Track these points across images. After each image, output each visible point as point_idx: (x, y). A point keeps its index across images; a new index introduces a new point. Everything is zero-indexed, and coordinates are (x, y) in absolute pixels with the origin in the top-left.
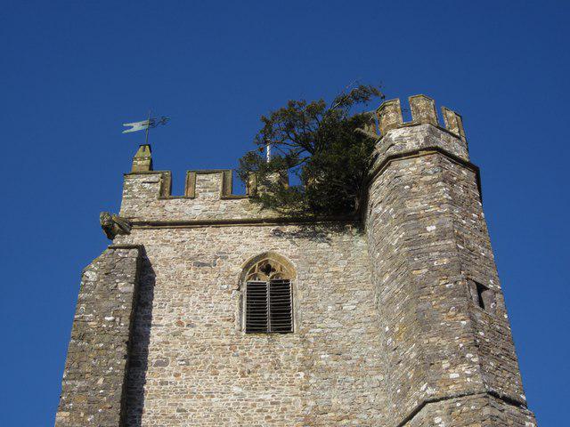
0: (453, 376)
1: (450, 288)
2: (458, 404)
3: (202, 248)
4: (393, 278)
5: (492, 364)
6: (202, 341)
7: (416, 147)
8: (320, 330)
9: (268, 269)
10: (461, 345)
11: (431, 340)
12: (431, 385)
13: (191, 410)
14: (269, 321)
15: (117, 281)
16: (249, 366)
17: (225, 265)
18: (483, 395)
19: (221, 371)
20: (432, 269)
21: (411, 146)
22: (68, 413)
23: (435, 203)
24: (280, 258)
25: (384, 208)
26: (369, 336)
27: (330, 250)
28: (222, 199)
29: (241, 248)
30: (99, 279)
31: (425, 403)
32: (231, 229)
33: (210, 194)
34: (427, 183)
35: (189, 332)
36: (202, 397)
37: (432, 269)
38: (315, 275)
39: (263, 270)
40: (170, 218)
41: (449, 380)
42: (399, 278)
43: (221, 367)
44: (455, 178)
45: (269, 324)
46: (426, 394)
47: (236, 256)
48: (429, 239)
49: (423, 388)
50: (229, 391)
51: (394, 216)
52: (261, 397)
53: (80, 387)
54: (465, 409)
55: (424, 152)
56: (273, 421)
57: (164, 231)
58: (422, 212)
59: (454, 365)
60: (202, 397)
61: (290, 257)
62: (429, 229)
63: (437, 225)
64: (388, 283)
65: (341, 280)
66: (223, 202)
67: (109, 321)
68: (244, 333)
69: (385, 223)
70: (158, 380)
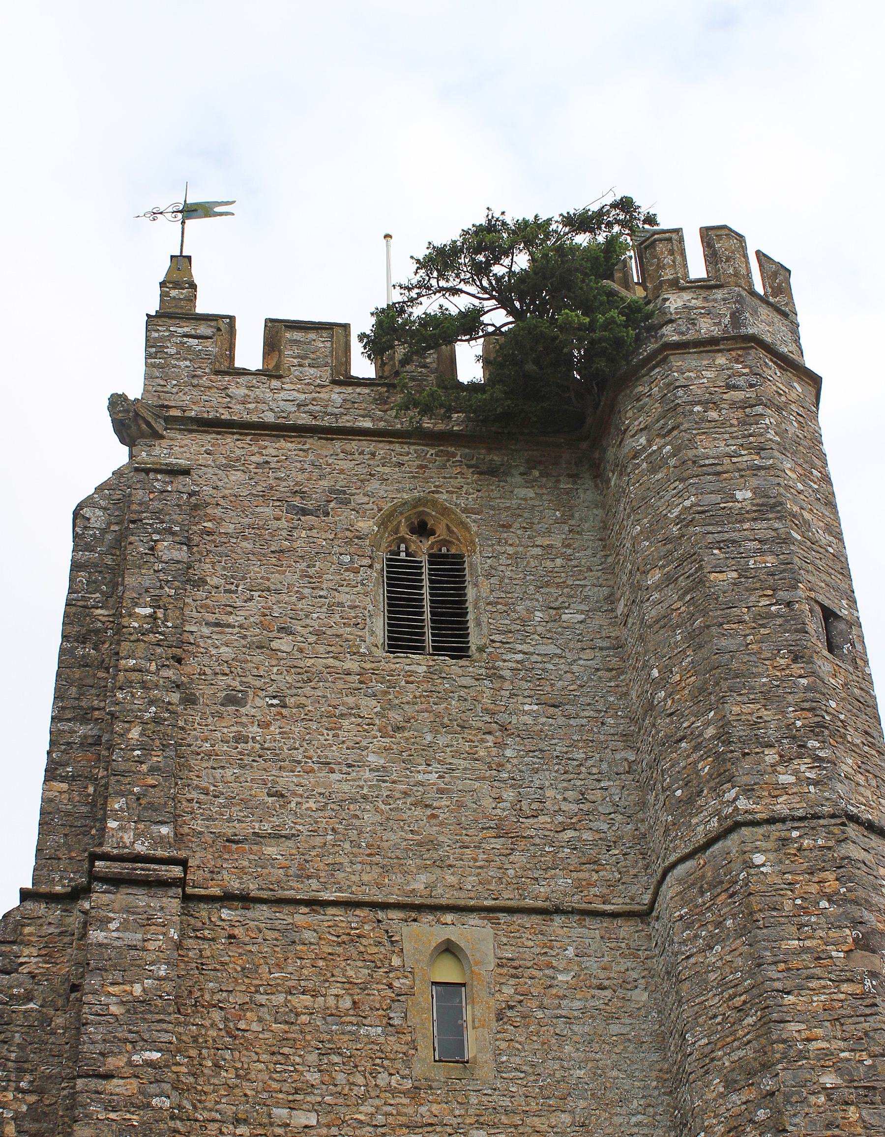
0: (786, 779)
1: (778, 615)
2: (795, 834)
3: (300, 477)
4: (669, 580)
5: (850, 761)
6: (309, 662)
7: (716, 332)
8: (519, 657)
9: (422, 529)
10: (799, 723)
11: (746, 709)
12: (748, 791)
13: (294, 794)
14: (428, 631)
15: (156, 537)
16: (395, 716)
17: (343, 516)
18: (838, 821)
19: (345, 723)
20: (743, 573)
21: (706, 328)
22: (64, 786)
23: (749, 447)
24: (445, 511)
25: (650, 442)
26: (609, 675)
27: (537, 503)
28: (334, 382)
29: (374, 485)
30: (109, 524)
31: (737, 825)
32: (353, 445)
33: (312, 371)
34: (733, 405)
35: (284, 644)
36: (312, 771)
37: (743, 573)
38: (510, 550)
39: (413, 531)
40: (239, 413)
41: (777, 786)
42: (683, 583)
43: (342, 715)
44: (783, 399)
45: (428, 637)
46: (736, 809)
47: (366, 499)
48: (741, 517)
49: (730, 795)
50: (361, 763)
51: (673, 462)
52: (420, 777)
53: (85, 737)
54: (806, 843)
55: (730, 345)
56: (441, 824)
57: (229, 439)
58: (726, 461)
59: (785, 759)
60: (312, 771)
61: (465, 510)
62: (739, 495)
63: (754, 491)
64: (658, 587)
65: (559, 562)
66: (338, 389)
67: (146, 617)
68: (379, 653)
69: (653, 470)
70: (231, 732)
